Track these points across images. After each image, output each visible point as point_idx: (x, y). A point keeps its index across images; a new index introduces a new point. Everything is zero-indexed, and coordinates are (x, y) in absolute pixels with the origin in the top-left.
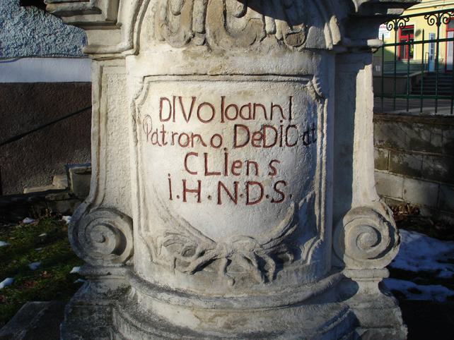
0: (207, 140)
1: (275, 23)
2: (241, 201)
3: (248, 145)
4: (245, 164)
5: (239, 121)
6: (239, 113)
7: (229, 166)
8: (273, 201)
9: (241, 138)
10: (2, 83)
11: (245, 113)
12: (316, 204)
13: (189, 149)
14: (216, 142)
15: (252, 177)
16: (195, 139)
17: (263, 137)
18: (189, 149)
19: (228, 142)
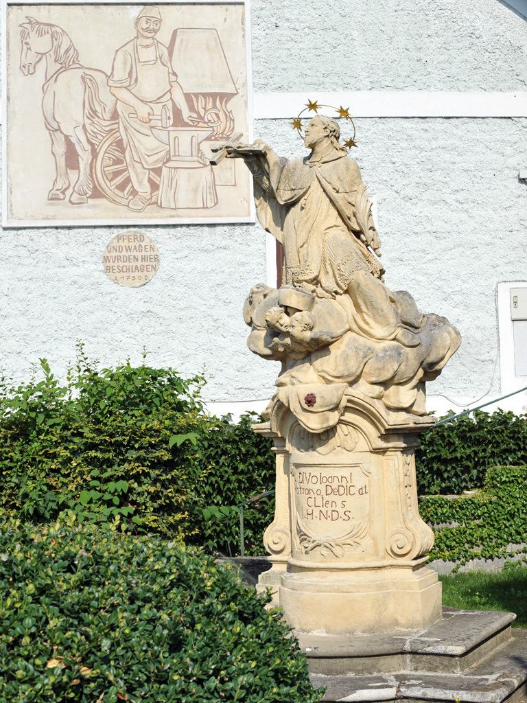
0: (315, 491)
1: (358, 223)
2: (329, 519)
3: (335, 285)
4: (330, 502)
5: (328, 484)
6: (327, 480)
7: (324, 502)
8: (344, 520)
9: (329, 492)
10: (30, 423)
11: (330, 479)
12: (121, 177)
13: (309, 496)
14: (319, 492)
15: (334, 508)
16: (336, 478)
17: (338, 491)
18: (309, 496)
19: (323, 492)
